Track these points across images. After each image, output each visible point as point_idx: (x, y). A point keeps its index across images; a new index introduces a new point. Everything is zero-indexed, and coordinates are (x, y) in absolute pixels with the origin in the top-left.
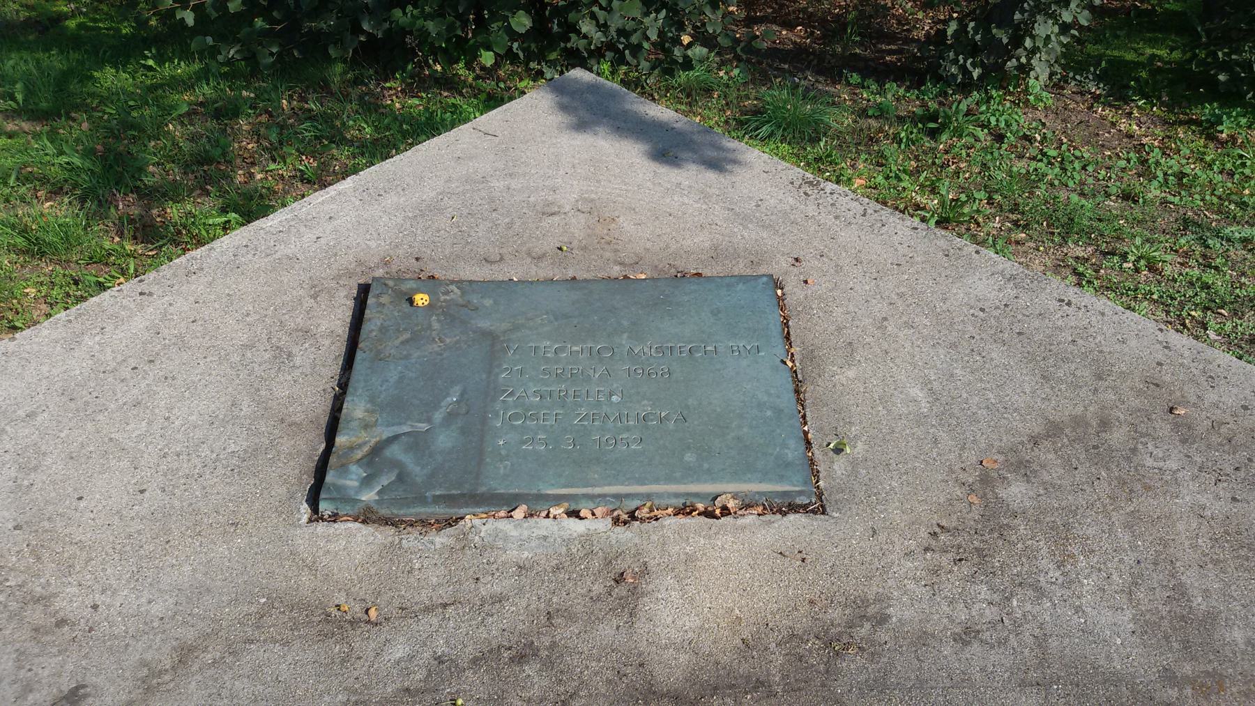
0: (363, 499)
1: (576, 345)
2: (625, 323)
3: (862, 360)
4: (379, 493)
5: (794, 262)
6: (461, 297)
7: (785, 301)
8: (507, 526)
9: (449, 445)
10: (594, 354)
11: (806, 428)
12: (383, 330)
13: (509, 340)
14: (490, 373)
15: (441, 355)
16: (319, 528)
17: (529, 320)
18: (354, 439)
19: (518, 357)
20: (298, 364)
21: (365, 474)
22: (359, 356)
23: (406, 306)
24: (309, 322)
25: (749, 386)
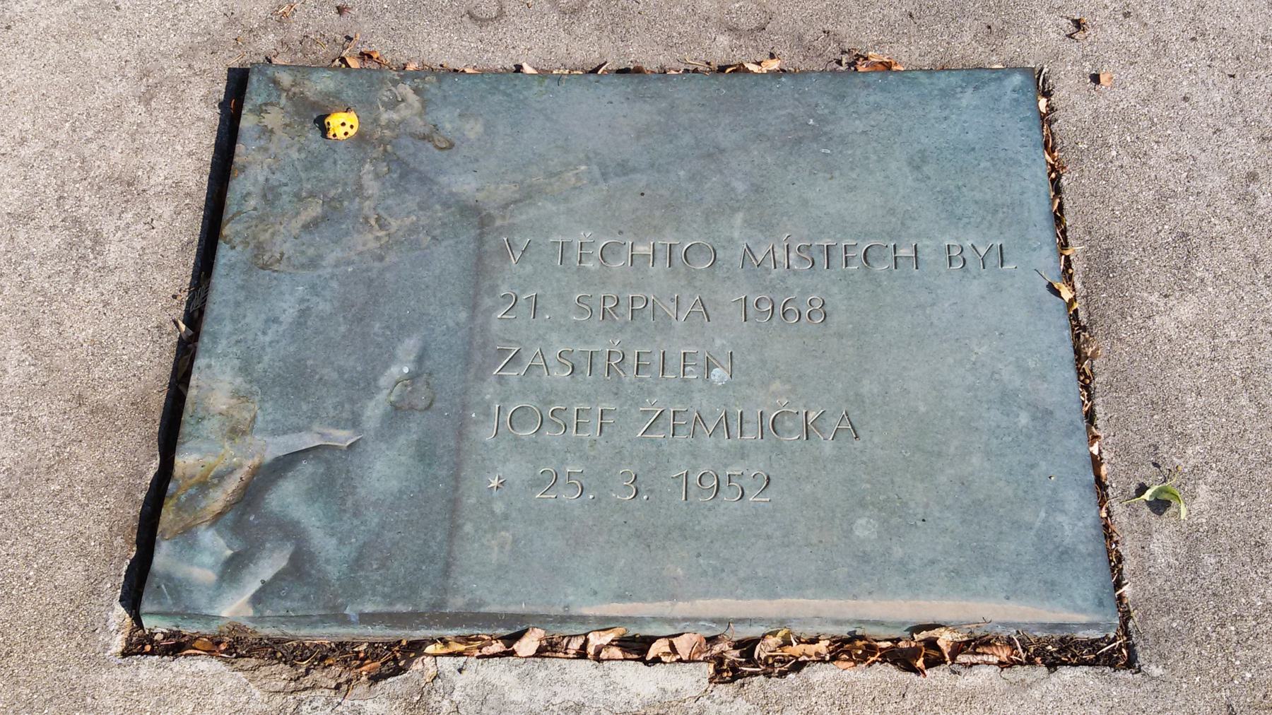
0: (224, 614)
1: (642, 241)
2: (740, 187)
3: (1209, 277)
4: (257, 599)
5: (1072, 28)
6: (420, 115)
7: (1055, 127)
8: (504, 678)
9: (394, 485)
10: (677, 262)
11: (1095, 450)
12: (270, 194)
13: (511, 228)
14: (474, 307)
15: (381, 259)
16: (142, 672)
17: (551, 175)
18: (211, 460)
19: (529, 268)
20: (111, 263)
21: (229, 552)
22: (224, 255)
23: (314, 135)
24: (135, 161)
25: (984, 349)
